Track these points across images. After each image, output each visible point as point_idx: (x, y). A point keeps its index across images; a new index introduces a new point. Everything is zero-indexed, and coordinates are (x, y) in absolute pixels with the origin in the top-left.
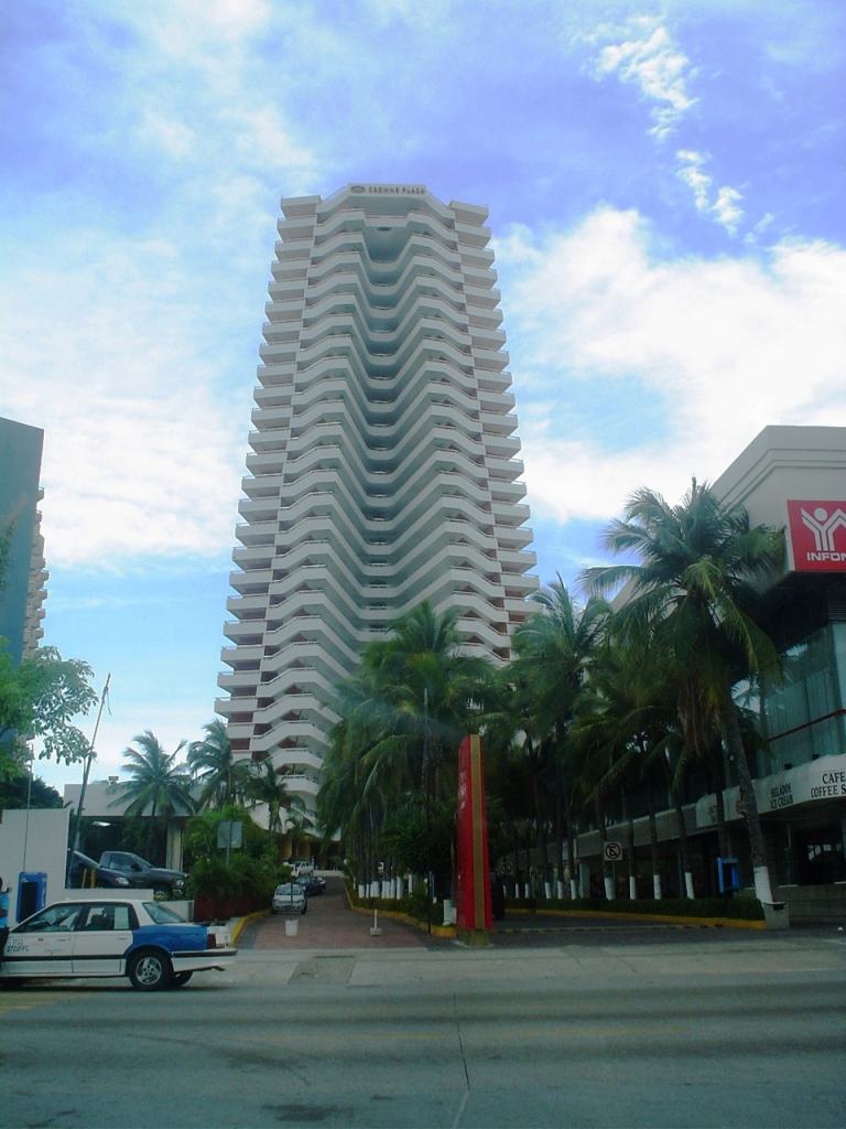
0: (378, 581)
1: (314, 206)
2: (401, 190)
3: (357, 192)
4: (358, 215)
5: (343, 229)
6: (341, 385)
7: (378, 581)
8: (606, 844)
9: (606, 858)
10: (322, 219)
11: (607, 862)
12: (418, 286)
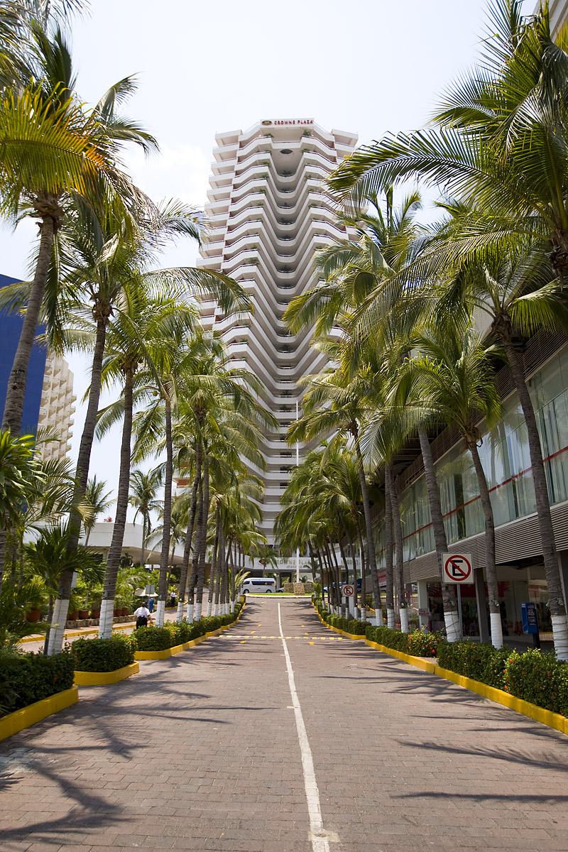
0: (286, 393)
1: (237, 137)
2: (296, 122)
3: (267, 124)
4: (269, 140)
5: (257, 151)
6: (262, 183)
7: (286, 393)
8: (446, 557)
9: (447, 580)
10: (242, 145)
11: (448, 586)
12: (315, 243)
